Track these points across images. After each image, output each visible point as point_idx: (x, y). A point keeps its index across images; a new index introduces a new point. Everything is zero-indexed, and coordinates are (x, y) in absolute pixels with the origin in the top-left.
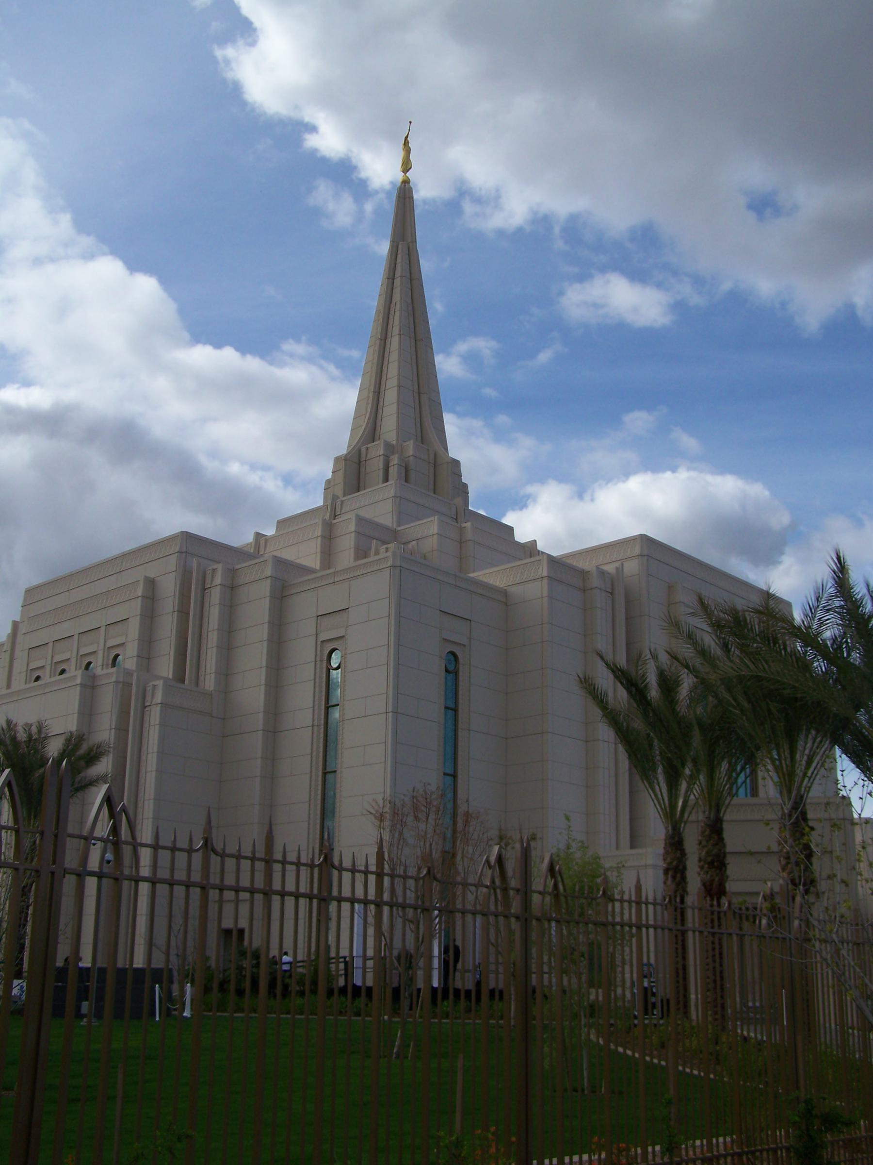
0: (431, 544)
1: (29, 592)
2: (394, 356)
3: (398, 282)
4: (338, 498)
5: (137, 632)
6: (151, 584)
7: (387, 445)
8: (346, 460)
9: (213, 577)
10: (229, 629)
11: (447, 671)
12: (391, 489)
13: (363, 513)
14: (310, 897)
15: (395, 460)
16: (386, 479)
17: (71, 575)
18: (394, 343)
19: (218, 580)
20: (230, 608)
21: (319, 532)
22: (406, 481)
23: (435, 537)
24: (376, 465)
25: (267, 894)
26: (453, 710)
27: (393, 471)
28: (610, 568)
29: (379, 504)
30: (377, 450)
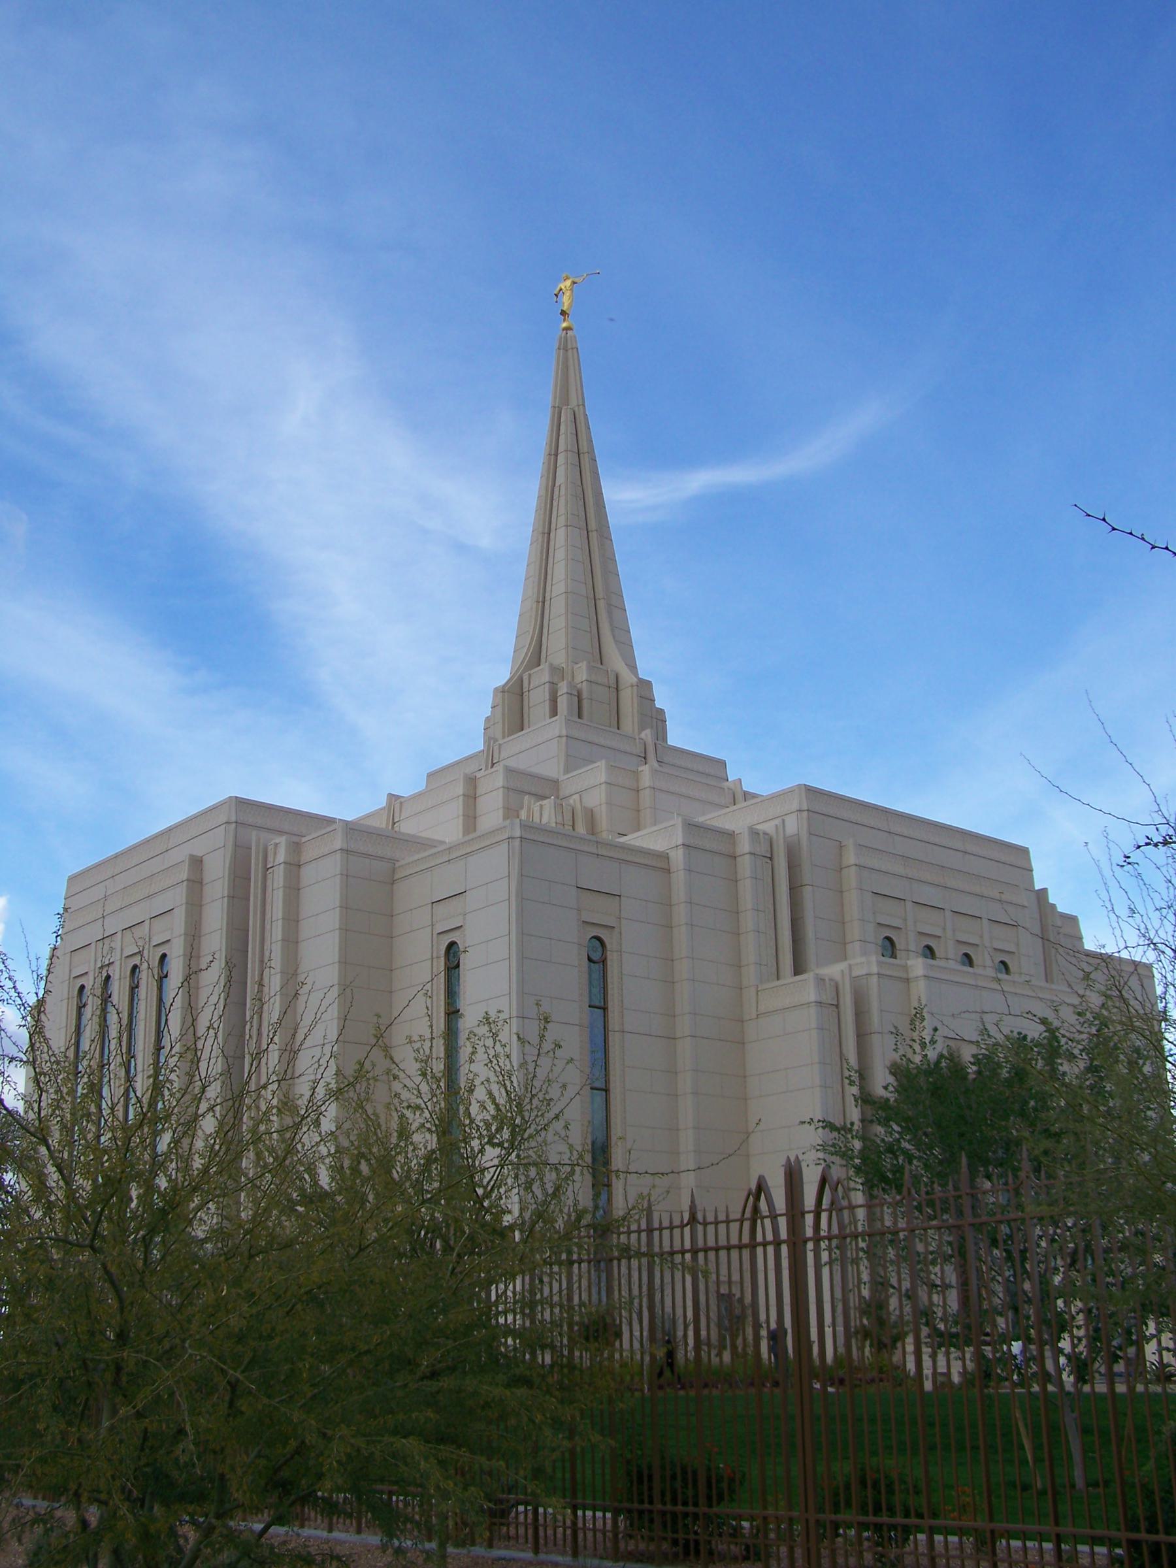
0: (596, 799)
1: (72, 879)
2: (560, 554)
3: (561, 459)
4: (496, 740)
5: (183, 924)
6: (197, 863)
7: (556, 671)
8: (503, 692)
9: (275, 854)
10: (292, 920)
11: (590, 960)
12: (557, 727)
13: (512, 763)
14: (740, 1247)
15: (563, 688)
16: (554, 712)
17: (116, 856)
18: (560, 536)
19: (281, 857)
20: (294, 890)
21: (460, 789)
22: (580, 716)
23: (603, 786)
24: (538, 698)
25: (753, 1246)
26: (601, 1007)
27: (563, 703)
28: (768, 827)
29: (542, 746)
30: (542, 676)
